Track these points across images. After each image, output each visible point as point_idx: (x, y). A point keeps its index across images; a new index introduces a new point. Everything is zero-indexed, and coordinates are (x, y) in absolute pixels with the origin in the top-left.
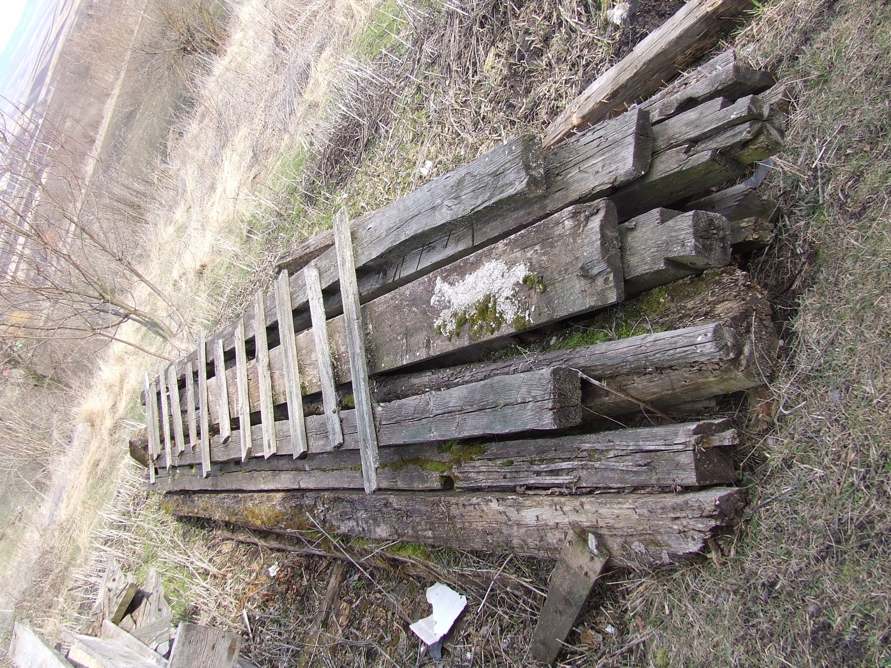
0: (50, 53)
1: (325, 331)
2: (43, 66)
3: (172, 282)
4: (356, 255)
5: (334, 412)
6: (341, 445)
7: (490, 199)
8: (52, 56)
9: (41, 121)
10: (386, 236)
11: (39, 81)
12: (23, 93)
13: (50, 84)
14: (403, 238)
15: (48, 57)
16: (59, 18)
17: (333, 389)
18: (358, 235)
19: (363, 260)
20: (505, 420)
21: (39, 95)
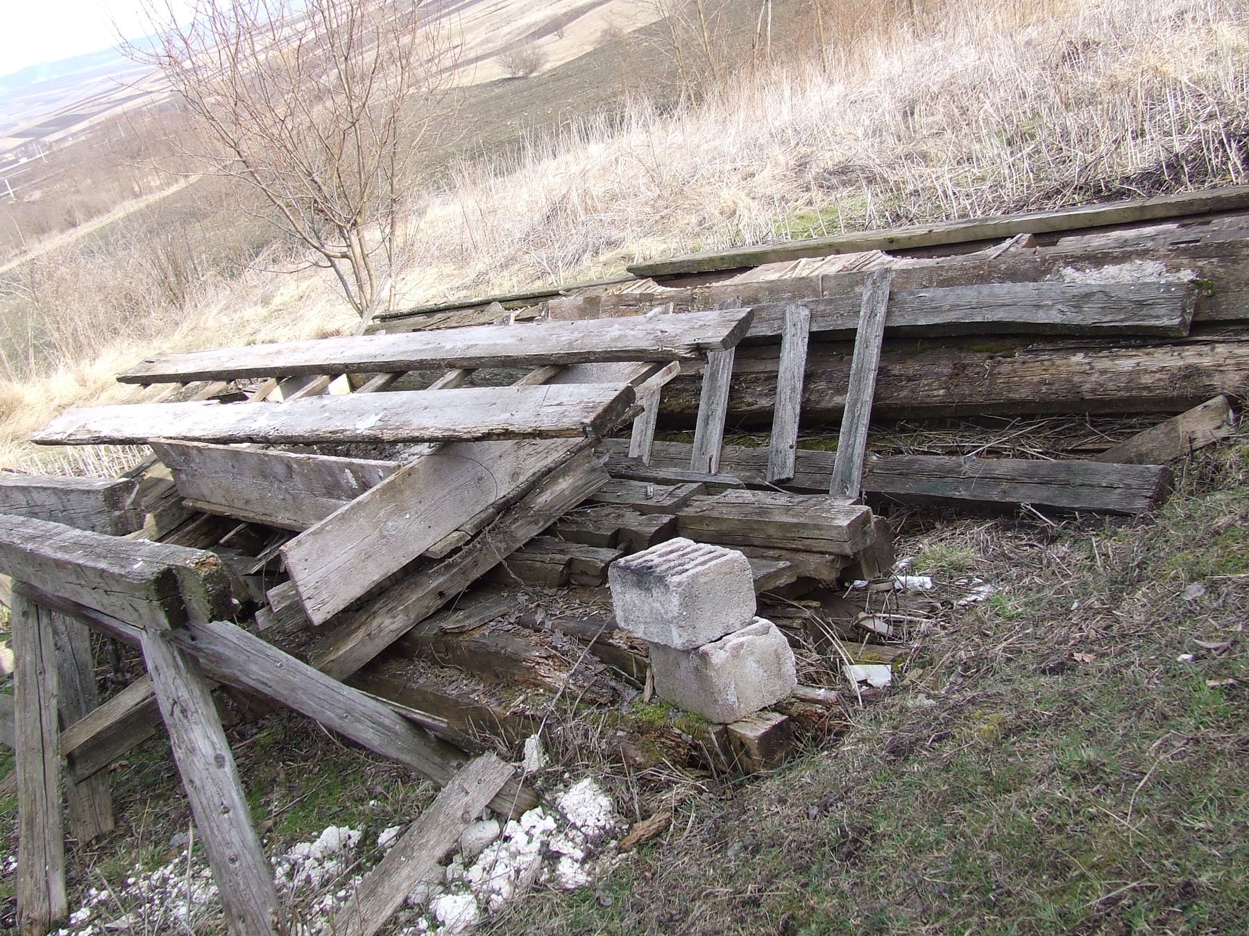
0: (102, 107)
1: (802, 370)
2: (81, 112)
3: (615, 234)
4: (889, 314)
5: (791, 447)
6: (788, 479)
7: (1122, 321)
8: (97, 113)
9: (24, 160)
10: (949, 310)
11: (63, 122)
12: (29, 118)
13: (74, 135)
14: (979, 319)
15: (96, 109)
16: (146, 85)
17: (796, 426)
18: (899, 297)
19: (899, 321)
20: (1077, 497)
21: (48, 134)
